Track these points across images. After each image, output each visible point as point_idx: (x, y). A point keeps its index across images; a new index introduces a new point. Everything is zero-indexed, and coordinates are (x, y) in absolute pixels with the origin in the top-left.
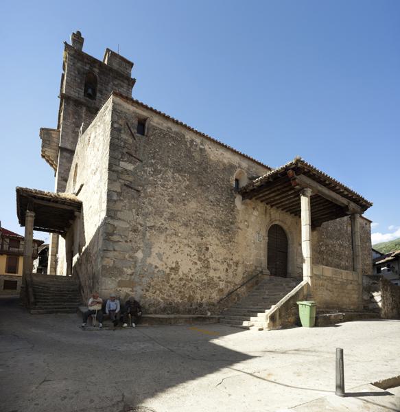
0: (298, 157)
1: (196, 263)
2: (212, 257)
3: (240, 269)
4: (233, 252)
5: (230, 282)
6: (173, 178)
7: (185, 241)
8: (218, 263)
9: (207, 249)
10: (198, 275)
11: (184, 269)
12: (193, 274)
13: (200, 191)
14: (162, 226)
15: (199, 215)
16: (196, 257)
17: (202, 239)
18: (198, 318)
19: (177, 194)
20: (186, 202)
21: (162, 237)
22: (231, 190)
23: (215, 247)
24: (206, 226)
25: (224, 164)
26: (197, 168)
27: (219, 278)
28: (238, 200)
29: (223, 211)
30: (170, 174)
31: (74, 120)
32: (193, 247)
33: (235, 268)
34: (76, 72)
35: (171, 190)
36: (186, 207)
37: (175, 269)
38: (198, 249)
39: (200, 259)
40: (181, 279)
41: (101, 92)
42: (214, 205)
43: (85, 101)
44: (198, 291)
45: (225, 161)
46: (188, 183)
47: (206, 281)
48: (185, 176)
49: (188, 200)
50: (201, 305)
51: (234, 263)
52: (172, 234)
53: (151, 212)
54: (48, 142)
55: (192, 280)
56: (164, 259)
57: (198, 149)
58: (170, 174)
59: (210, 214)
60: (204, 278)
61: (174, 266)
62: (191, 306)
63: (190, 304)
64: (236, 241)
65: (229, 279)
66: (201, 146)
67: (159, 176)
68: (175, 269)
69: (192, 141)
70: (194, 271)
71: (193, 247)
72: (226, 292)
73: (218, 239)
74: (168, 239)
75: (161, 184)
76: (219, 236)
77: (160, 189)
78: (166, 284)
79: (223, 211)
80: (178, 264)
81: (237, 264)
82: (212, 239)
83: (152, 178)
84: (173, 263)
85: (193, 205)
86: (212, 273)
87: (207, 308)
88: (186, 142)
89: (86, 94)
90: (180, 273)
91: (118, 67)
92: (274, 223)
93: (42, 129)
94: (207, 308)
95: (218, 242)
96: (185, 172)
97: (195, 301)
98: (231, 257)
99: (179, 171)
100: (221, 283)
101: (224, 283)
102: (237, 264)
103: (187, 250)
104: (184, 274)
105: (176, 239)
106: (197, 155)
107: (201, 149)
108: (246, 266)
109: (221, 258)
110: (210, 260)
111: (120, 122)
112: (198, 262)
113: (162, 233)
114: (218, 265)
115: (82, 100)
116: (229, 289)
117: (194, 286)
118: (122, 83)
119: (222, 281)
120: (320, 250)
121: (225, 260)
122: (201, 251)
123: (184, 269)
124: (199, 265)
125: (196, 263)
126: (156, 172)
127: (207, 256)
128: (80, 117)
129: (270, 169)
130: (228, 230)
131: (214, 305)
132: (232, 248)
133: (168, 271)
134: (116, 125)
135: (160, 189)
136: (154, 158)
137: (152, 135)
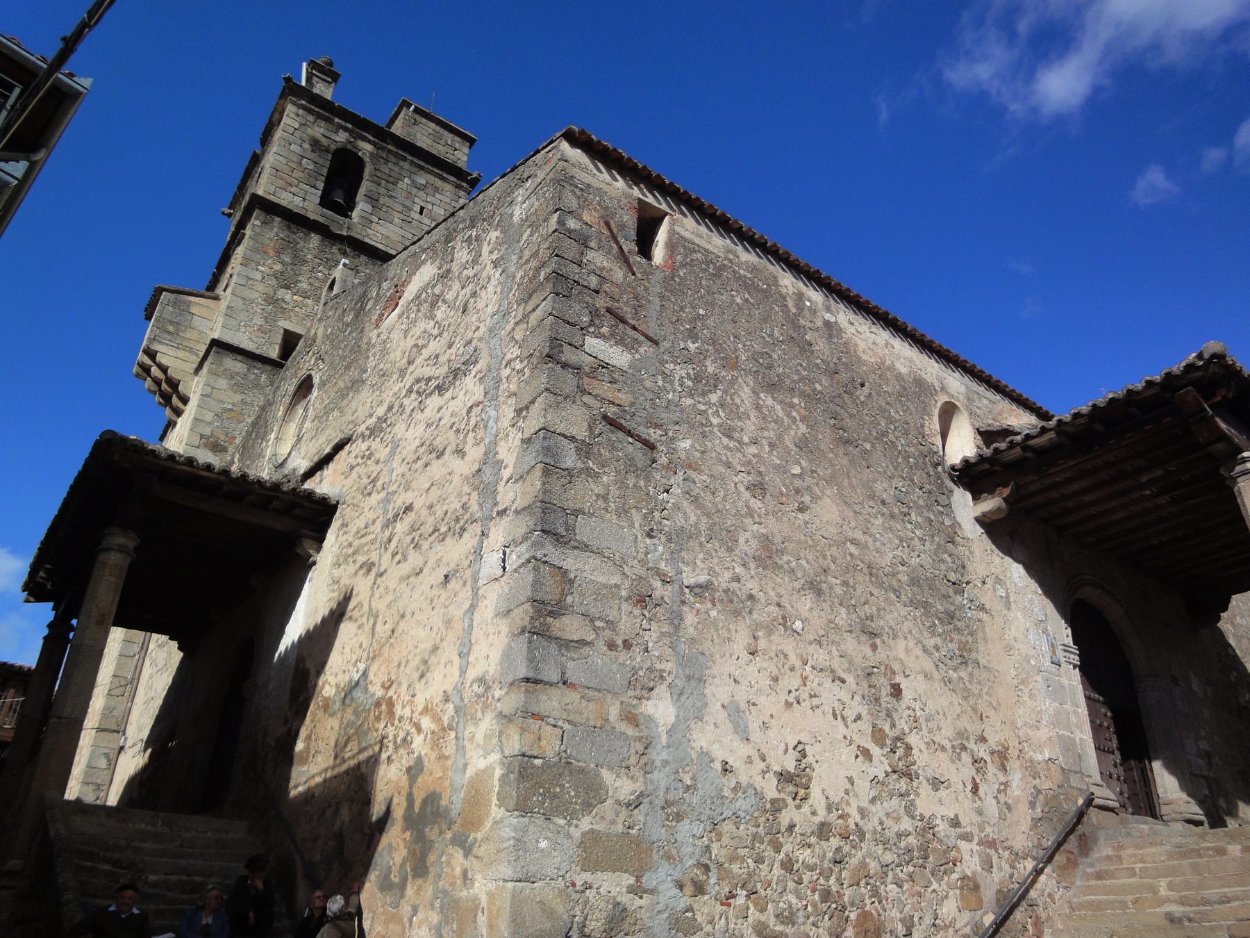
0: (1213, 347)
9: (897, 691)
15: (853, 549)
31: (278, 267)
32: (850, 679)
34: (306, 146)
41: (373, 199)
42: (892, 516)
43: (321, 220)
54: (171, 328)
67: (714, 398)
68: (795, 781)
74: (762, 644)
77: (719, 442)
83: (689, 401)
88: (784, 298)
89: (326, 201)
91: (430, 142)
108: (1032, 770)
111: (586, 217)
115: (312, 216)
117: (873, 866)
118: (439, 183)
126: (702, 383)
128: (298, 260)
134: (572, 224)
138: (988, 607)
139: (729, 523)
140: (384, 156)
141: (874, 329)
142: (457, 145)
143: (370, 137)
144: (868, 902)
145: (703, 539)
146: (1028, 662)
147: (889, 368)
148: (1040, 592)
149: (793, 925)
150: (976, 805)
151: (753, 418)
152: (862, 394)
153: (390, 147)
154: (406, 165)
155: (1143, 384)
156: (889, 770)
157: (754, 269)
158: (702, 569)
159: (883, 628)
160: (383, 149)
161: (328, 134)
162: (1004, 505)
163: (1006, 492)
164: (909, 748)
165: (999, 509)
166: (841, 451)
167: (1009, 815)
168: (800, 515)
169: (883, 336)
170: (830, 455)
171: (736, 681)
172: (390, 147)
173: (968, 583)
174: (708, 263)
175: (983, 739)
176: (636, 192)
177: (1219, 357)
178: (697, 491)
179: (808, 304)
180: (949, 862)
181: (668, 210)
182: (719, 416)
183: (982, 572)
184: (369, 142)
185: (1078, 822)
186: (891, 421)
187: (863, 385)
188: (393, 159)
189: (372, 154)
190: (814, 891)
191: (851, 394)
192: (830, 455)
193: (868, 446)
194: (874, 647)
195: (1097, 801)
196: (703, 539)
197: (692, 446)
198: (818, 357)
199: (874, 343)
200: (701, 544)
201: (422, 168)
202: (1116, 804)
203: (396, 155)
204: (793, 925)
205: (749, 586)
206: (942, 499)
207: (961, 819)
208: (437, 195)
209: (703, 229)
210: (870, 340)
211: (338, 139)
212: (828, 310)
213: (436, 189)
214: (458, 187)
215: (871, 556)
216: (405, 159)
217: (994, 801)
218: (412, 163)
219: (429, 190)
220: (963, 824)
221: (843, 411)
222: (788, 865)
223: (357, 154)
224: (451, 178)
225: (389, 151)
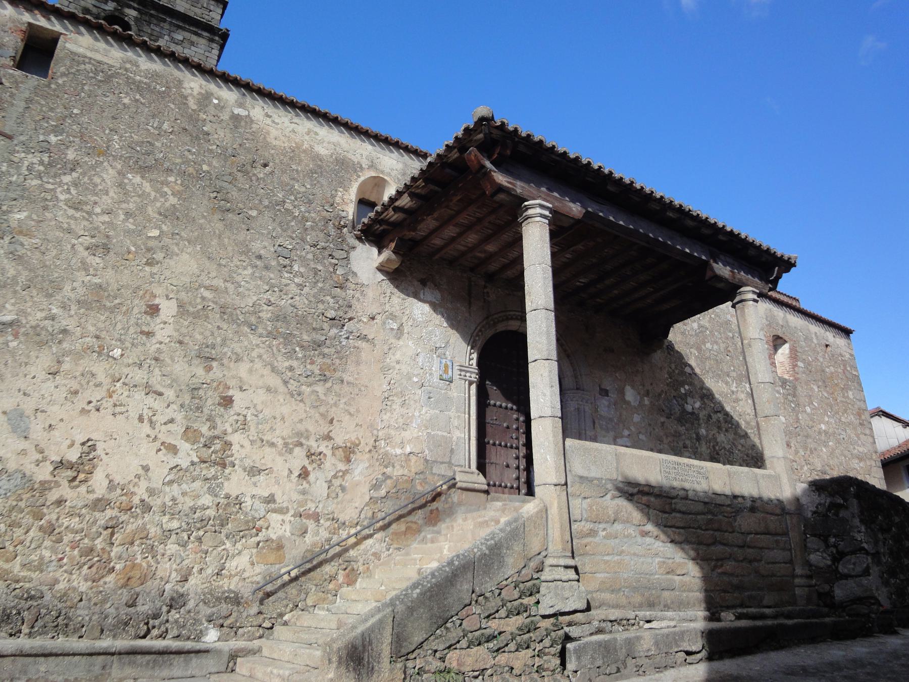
0: (483, 110)
1: (173, 449)
2: (243, 425)
3: (361, 470)
4: (333, 412)
5: (316, 517)
6: (121, 185)
7: (139, 376)
8: (267, 450)
9: (227, 402)
10: (175, 490)
11: (117, 465)
12: (157, 484)
13: (220, 226)
14: (47, 323)
15: (207, 294)
16: (178, 429)
17: (209, 369)
18: (133, 652)
19: (128, 232)
20: (159, 256)
21: (44, 360)
22: (340, 228)
23: (260, 397)
24: (229, 329)
25: (317, 157)
26: (215, 163)
27: (270, 499)
28: (367, 260)
29: (301, 286)
30: (109, 174)
32: (170, 394)
33: (342, 466)
35: (106, 218)
36: (155, 269)
37: (78, 469)
38: (187, 398)
39: (190, 434)
40: (99, 504)
42: (267, 268)
44: (172, 547)
45: (322, 151)
46: (173, 200)
47: (211, 513)
48: (167, 184)
49: (165, 249)
50: (176, 602)
51: (335, 448)
52: (90, 349)
53: (14, 278)
55: (146, 508)
56: (37, 430)
57: (225, 116)
58: (109, 174)
59: (250, 290)
60: (207, 500)
61: (73, 456)
62: (132, 604)
63: (125, 595)
64: (346, 378)
65: (311, 506)
66: (237, 111)
67: (67, 179)
68: (78, 469)
69: (206, 97)
70: (159, 474)
71: (170, 394)
72: (295, 552)
73: (274, 370)
74: (66, 367)
75: (67, 202)
76: (283, 364)
77: (64, 214)
78: (28, 520)
79: (301, 286)
80: (93, 448)
81: (348, 453)
82: (250, 371)
83: (36, 182)
84: (72, 445)
85: (185, 264)
86: (235, 484)
87: (206, 611)
88: (186, 98)
90: (99, 482)
91: (188, 6)
92: (501, 327)
93: (378, 268)
94: (206, 611)
95: (275, 381)
96: (169, 171)
97: (152, 585)
98: (324, 429)
99: (144, 170)
100: (274, 518)
101: (288, 517)
102: (348, 453)
103: (139, 402)
104: (112, 486)
105: (100, 369)
106: (222, 135)
107: (236, 118)
108: (387, 461)
109: (282, 431)
110: (236, 439)
112: (184, 447)
113: (41, 344)
114: (269, 457)
116: (309, 539)
117: (153, 531)
118: (194, 38)
119: (282, 511)
120: (684, 411)
121: (298, 440)
122: (199, 408)
123: (117, 465)
124: (187, 453)
125: (173, 449)
126: (56, 165)
127: (220, 428)
129: (425, 156)
130: (318, 345)
131: (236, 600)
132: (331, 399)
133: (44, 473)
135: (64, 214)
136: (56, 131)
137: (63, 75)
138: (370, 337)
139: (56, 275)
140: (147, 18)
141: (296, 120)
142: (212, 8)
143: (136, 5)
144: (139, 557)
145: (18, 288)
146: (410, 378)
147: (305, 151)
148: (445, 324)
149: (42, 572)
150: (300, 487)
151: (111, 194)
152: (261, 173)
153: (152, 12)
154: (166, 26)
155: (444, 148)
156: (196, 460)
157: (155, 76)
158: (11, 311)
159: (225, 354)
160: (146, 14)
161: (98, 4)
162: (394, 257)
163: (393, 245)
164: (229, 444)
165: (389, 260)
166: (217, 216)
167: (341, 495)
168: (147, 268)
169: (305, 125)
170: (202, 221)
171: (25, 394)
172: (152, 12)
173: (350, 319)
174: (96, 72)
175: (328, 437)
176: (27, 18)
177: (484, 121)
178: (24, 251)
179: (216, 101)
180: (253, 527)
181: (63, 31)
182: (70, 193)
183: (373, 309)
184: (135, 9)
185: (434, 499)
186: (291, 191)
187: (265, 165)
188: (155, 22)
189: (136, 18)
190: (73, 548)
191: (246, 173)
192: (202, 221)
193: (254, 213)
194: (209, 369)
195: (459, 485)
196: (18, 288)
197: (29, 217)
198: (214, 144)
199: (293, 131)
200: (15, 292)
201: (179, 27)
202: (486, 487)
203: (157, 18)
204: (42, 572)
205: (64, 323)
206: (339, 254)
207: (276, 497)
208: (193, 48)
209: (101, 45)
210: (282, 128)
211: (107, 8)
212: (241, 105)
213: (192, 43)
214: (211, 40)
215: (231, 298)
216: (165, 21)
217: (326, 485)
218: (171, 23)
219: (186, 44)
220: (278, 501)
221: (230, 186)
222: (50, 530)
223: (123, 20)
224: (205, 34)
225: (152, 15)
